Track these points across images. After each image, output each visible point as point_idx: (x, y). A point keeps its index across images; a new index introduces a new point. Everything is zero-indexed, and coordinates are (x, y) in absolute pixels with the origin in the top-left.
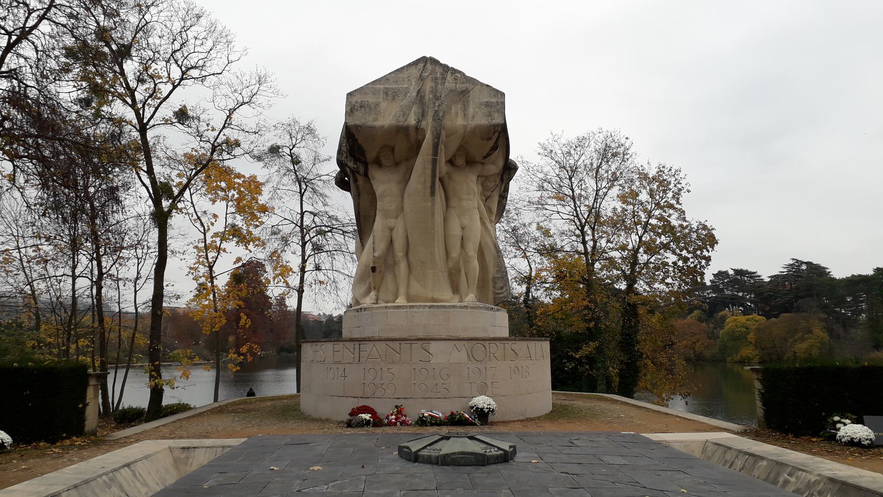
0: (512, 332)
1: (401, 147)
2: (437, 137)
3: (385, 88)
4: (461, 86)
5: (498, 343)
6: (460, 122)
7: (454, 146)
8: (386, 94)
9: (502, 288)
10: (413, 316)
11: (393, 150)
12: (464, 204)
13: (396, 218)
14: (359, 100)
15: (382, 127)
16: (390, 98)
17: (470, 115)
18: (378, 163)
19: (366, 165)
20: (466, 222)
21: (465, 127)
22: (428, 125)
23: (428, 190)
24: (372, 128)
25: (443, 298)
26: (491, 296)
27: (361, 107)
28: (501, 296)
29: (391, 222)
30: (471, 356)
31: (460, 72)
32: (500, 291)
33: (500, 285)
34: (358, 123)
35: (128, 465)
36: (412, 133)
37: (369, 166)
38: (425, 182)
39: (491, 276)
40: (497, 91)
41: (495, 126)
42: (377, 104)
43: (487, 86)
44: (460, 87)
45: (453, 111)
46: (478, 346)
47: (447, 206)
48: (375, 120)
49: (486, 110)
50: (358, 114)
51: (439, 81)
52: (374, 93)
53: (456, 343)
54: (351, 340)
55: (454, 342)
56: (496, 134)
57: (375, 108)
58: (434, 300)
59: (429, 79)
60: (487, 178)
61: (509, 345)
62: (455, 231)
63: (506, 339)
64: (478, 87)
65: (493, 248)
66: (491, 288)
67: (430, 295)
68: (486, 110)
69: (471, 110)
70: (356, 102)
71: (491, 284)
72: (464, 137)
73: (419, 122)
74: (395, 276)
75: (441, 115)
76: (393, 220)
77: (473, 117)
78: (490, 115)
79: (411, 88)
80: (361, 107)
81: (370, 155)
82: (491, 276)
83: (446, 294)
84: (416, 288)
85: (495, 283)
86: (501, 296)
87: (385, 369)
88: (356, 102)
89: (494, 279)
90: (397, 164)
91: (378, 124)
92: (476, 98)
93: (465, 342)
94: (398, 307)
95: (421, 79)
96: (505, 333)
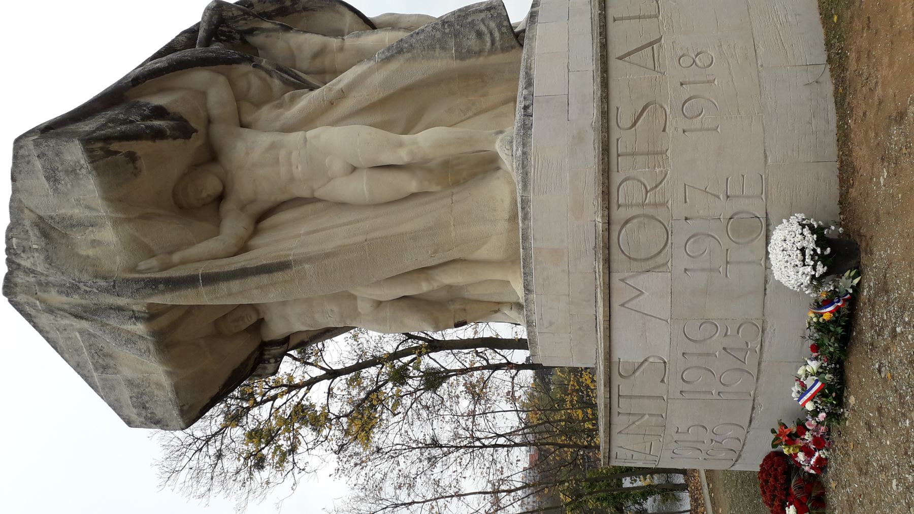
2: (153, 284)
3: (96, 369)
4: (33, 238)
5: (616, 178)
6: (108, 235)
7: (170, 230)
8: (105, 368)
9: (480, 34)
10: (551, 324)
12: (299, 170)
13: (354, 298)
14: (135, 411)
15: (169, 374)
16: (109, 361)
17: (87, 213)
20: (337, 166)
21: (116, 223)
22: (139, 305)
23: (278, 276)
24: (177, 389)
26: (498, 59)
27: (144, 408)
28: (497, 35)
30: (652, 263)
31: (8, 239)
32: (488, 38)
33: (471, 41)
35: (705, 191)
37: (267, 339)
39: (456, 64)
40: (15, 157)
42: (130, 383)
43: (13, 179)
44: (35, 240)
45: (91, 252)
46: (623, 238)
48: (159, 386)
49: (66, 182)
50: (159, 413)
52: (112, 388)
55: (615, 306)
56: (115, 146)
57: (138, 386)
59: (45, 296)
60: (240, 98)
62: (357, 188)
65: (394, 66)
66: (481, 60)
67: (502, 226)
68: (66, 182)
69: (77, 212)
70: (139, 412)
71: (471, 62)
72: (143, 217)
73: (135, 317)
74: (471, 285)
75: (102, 283)
76: (359, 302)
77: (88, 207)
78: (73, 172)
79: (78, 326)
80: (144, 408)
82: (456, 64)
83: (499, 192)
84: (491, 250)
85: (470, 53)
86: (497, 35)
87: (676, 437)
88: (139, 415)
89: (462, 55)
91: (166, 382)
93: (616, 277)
95: (51, 310)
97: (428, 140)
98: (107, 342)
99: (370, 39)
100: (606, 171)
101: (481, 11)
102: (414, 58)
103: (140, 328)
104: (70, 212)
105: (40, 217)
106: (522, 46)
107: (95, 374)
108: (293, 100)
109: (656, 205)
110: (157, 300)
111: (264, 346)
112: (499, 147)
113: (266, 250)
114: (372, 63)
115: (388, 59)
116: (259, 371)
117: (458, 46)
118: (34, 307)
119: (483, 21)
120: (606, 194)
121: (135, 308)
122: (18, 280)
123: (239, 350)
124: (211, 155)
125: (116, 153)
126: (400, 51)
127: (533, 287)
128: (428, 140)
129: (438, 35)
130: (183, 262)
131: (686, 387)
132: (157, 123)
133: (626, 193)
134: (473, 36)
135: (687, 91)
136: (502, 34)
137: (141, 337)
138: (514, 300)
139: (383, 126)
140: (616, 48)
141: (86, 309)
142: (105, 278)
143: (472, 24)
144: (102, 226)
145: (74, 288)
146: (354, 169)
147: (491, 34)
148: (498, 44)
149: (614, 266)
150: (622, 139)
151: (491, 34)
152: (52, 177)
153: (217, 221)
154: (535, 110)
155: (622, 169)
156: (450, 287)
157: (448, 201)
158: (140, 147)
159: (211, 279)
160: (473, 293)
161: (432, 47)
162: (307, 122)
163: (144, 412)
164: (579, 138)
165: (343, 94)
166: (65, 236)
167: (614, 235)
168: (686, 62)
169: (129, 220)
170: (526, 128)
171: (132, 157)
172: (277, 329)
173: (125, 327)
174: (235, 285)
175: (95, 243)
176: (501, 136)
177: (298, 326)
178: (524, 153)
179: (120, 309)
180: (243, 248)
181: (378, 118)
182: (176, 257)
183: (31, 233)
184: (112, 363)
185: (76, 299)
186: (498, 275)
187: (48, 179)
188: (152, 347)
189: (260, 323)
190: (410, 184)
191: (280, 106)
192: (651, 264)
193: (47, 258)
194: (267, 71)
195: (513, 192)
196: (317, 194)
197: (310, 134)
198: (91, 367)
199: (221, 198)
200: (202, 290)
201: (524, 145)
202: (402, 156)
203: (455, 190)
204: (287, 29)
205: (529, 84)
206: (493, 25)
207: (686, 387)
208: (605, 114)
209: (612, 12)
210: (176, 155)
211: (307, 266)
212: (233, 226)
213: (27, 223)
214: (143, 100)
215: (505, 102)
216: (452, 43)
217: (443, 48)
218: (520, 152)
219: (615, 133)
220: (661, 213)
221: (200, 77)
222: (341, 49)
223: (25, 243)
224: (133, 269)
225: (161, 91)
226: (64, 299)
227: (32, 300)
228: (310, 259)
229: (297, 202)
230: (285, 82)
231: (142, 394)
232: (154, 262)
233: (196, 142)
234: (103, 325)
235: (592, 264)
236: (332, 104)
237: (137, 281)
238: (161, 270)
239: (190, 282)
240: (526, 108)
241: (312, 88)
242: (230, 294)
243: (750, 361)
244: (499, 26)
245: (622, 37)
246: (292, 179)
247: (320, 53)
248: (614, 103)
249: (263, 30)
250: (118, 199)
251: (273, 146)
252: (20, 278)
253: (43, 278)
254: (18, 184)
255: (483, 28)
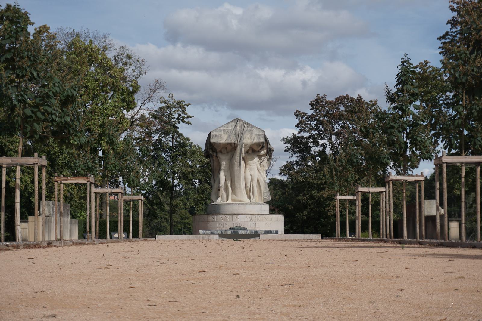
1: (229, 148)
11: (226, 148)
12: (252, 167)
15: (222, 143)
18: (221, 152)
19: (217, 153)
20: (252, 173)
30: (251, 220)
36: (233, 145)
39: (262, 192)
42: (221, 135)
47: (265, 136)
48: (221, 140)
65: (263, 181)
69: (254, 136)
81: (218, 150)
85: (264, 194)
90: (228, 153)
91: (221, 142)
92: (255, 132)
94: (228, 204)
96: (269, 213)
120: (259, 214)
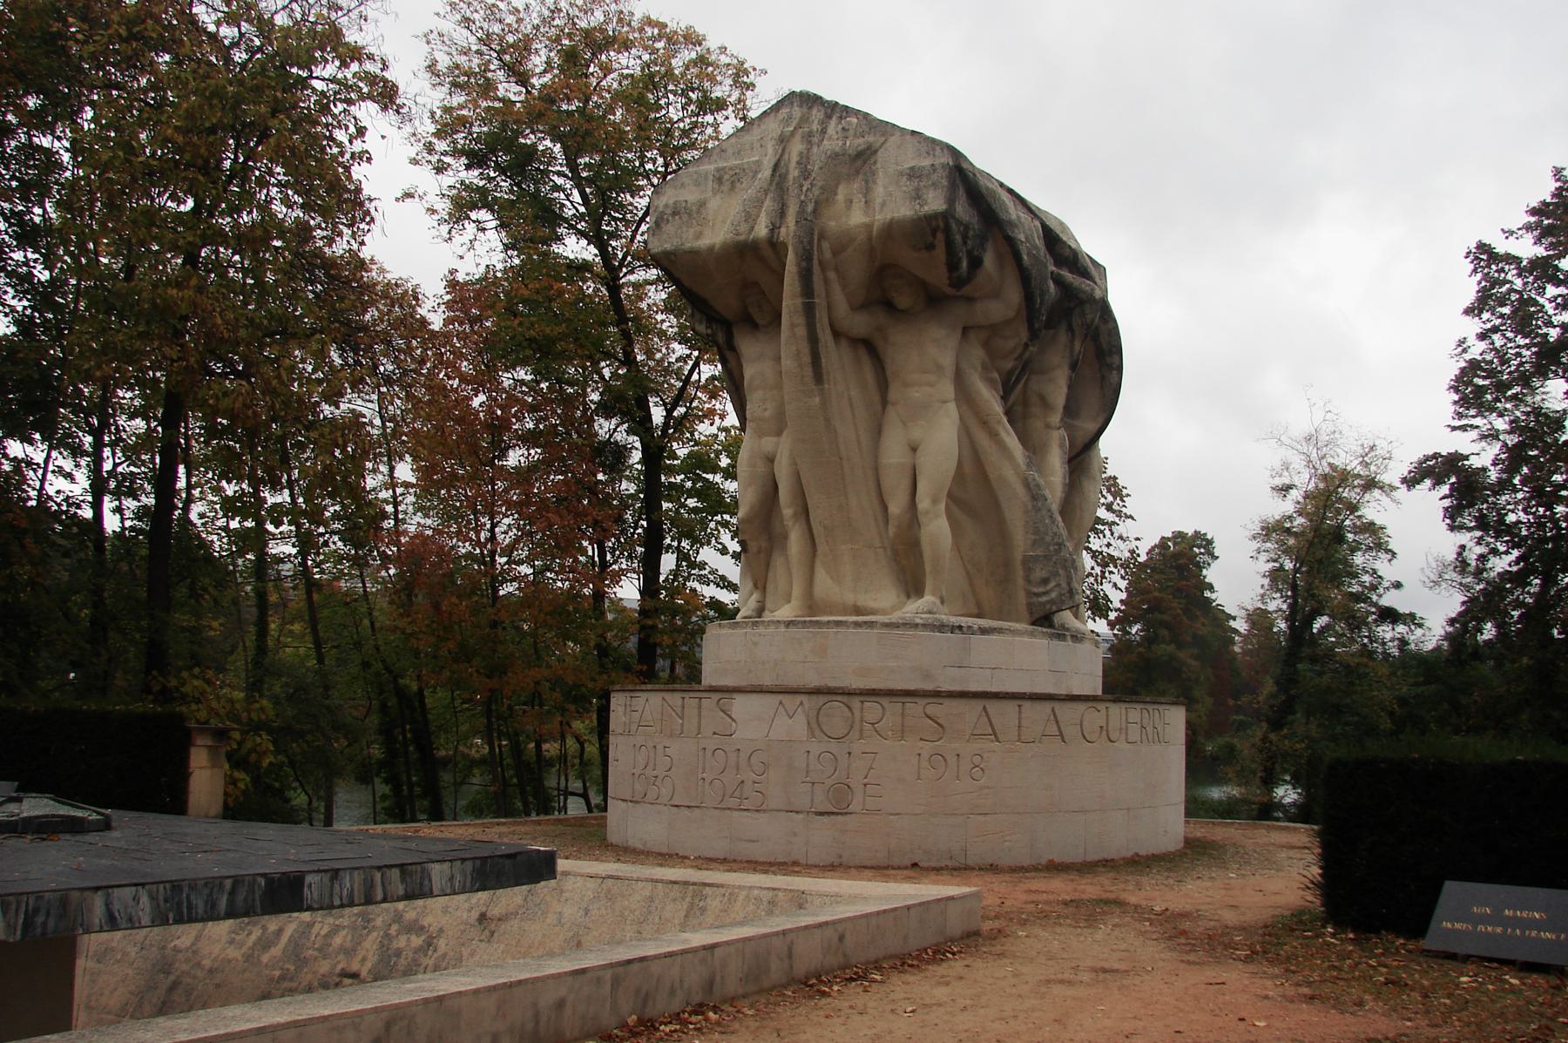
0: (1108, 688)
2: (806, 257)
3: (718, 170)
5: (885, 701)
6: (857, 218)
7: (857, 270)
8: (720, 180)
9: (1045, 581)
10: (755, 644)
12: (916, 394)
13: (779, 433)
14: (671, 202)
15: (711, 249)
16: (725, 188)
17: (879, 201)
20: (916, 433)
22: (789, 230)
23: (808, 371)
24: (694, 253)
25: (872, 604)
26: (1021, 598)
27: (674, 214)
28: (1044, 599)
29: (768, 443)
30: (815, 725)
32: (1041, 590)
33: (1039, 573)
34: (668, 246)
38: (798, 353)
39: (1018, 555)
40: (933, 141)
41: (930, 218)
42: (702, 204)
43: (913, 132)
45: (840, 197)
46: (836, 705)
48: (699, 236)
51: (815, 140)
53: (786, 699)
54: (714, 690)
55: (781, 697)
56: (940, 236)
57: (698, 212)
58: (858, 611)
59: (798, 137)
61: (1094, 717)
62: (893, 452)
63: (1094, 699)
64: (894, 140)
65: (1020, 490)
66: (1020, 582)
67: (850, 598)
68: (907, 186)
69: (879, 191)
71: (1020, 572)
73: (774, 229)
75: (810, 208)
76: (773, 440)
77: (883, 204)
78: (917, 196)
80: (674, 214)
83: (884, 597)
85: (1028, 570)
86: (1044, 599)
87: (660, 747)
88: (666, 206)
89: (1028, 562)
91: (704, 242)
92: (893, 160)
93: (804, 698)
95: (783, 140)
97: (937, 529)
98: (749, 190)
99: (1056, 462)
100: (890, 693)
101: (1069, 584)
102: (1026, 512)
103: (762, 231)
104: (880, 182)
105: (876, 152)
106: (1033, 624)
107: (712, 167)
108: (991, 382)
109: (861, 731)
110: (791, 258)
111: (728, 326)
112: (928, 599)
113: (836, 358)
114: (1024, 467)
115: (1027, 484)
116: (698, 316)
117: (1036, 559)
118: (787, 121)
119: (1058, 585)
121: (783, 230)
122: (814, 111)
123: (726, 302)
124: (934, 301)
125: (934, 236)
126: (1034, 498)
127: (792, 630)
128: (937, 529)
129: (1048, 539)
130: (826, 281)
131: (709, 753)
132: (965, 264)
133: (872, 709)
134: (1044, 574)
135: (952, 760)
136: (1044, 604)
137: (752, 228)
138: (769, 605)
139: (959, 475)
140: (994, 707)
141: (784, 177)
142: (815, 211)
143: (1056, 574)
144: (866, 214)
145: (805, 174)
146: (914, 450)
147: (1044, 593)
148: (1035, 599)
149: (814, 697)
150: (915, 708)
151: (1044, 593)
152: (913, 174)
153: (863, 307)
154: (957, 636)
155: (893, 707)
156: (786, 537)
157: (877, 543)
158: (940, 252)
159: (809, 310)
160: (778, 562)
161: (1036, 531)
162: (964, 396)
163: (669, 211)
164: (927, 676)
165: (994, 435)
166: (857, 172)
167: (839, 698)
168: (977, 760)
169: (870, 239)
170: (941, 627)
171: (930, 247)
172: (749, 348)
173: (763, 214)
174: (802, 331)
175: (849, 202)
176: (938, 602)
177: (749, 372)
178: (917, 625)
179: (782, 214)
180: (837, 334)
181: (968, 468)
182: (832, 275)
183: (861, 140)
184: (725, 188)
185: (794, 173)
186: (797, 591)
187: (912, 169)
188: (741, 238)
189: (753, 326)
190: (896, 507)
191: (985, 368)
192: (815, 726)
193: (837, 155)
194: (1021, 356)
195: (884, 612)
196: (889, 408)
197: (952, 406)
198: (722, 164)
199: (889, 306)
200: (799, 301)
201: (924, 625)
202: (923, 503)
203: (889, 552)
204: (1073, 366)
205: (984, 631)
206: (1053, 595)
207: (709, 753)
208: (937, 694)
209: (1027, 705)
210: (938, 276)
211: (817, 400)
212: (860, 324)
213: (871, 139)
214: (989, 246)
215: (979, 605)
216: (1038, 552)
217: (1035, 542)
218: (918, 621)
219: (922, 701)
220: (855, 734)
221: (1014, 295)
222: (1048, 426)
223: (851, 132)
224: (822, 236)
225: (1000, 258)
226: (795, 159)
227: (795, 123)
228: (825, 403)
229: (883, 385)
230: (1010, 373)
231: (690, 215)
232: (828, 255)
233: (950, 291)
234: (766, 192)
235: (813, 681)
236: (985, 423)
237: (811, 242)
238: (820, 263)
239: (807, 290)
240: (960, 627)
241: (1004, 398)
242: (793, 326)
243: (733, 802)
244: (1052, 602)
245: (1005, 713)
246: (906, 385)
247: (1046, 404)
248: (947, 702)
249: (1072, 341)
250: (891, 231)
251: (939, 368)
252: (817, 114)
253: (815, 140)
254: (908, 137)
255: (1052, 584)
